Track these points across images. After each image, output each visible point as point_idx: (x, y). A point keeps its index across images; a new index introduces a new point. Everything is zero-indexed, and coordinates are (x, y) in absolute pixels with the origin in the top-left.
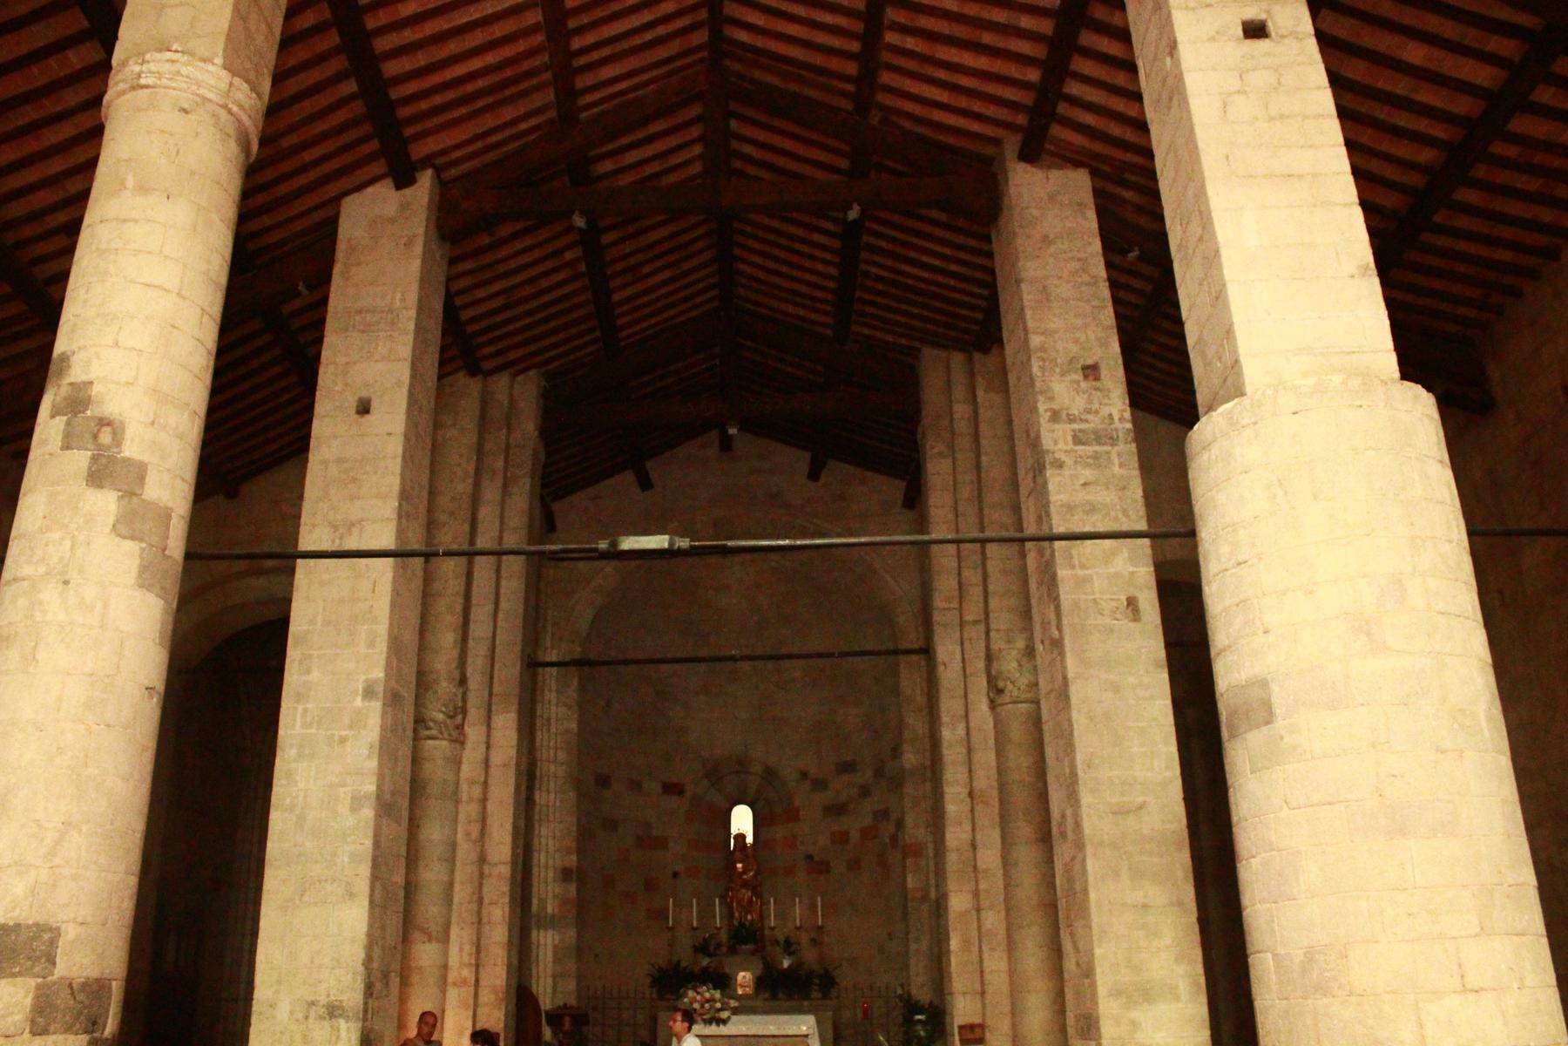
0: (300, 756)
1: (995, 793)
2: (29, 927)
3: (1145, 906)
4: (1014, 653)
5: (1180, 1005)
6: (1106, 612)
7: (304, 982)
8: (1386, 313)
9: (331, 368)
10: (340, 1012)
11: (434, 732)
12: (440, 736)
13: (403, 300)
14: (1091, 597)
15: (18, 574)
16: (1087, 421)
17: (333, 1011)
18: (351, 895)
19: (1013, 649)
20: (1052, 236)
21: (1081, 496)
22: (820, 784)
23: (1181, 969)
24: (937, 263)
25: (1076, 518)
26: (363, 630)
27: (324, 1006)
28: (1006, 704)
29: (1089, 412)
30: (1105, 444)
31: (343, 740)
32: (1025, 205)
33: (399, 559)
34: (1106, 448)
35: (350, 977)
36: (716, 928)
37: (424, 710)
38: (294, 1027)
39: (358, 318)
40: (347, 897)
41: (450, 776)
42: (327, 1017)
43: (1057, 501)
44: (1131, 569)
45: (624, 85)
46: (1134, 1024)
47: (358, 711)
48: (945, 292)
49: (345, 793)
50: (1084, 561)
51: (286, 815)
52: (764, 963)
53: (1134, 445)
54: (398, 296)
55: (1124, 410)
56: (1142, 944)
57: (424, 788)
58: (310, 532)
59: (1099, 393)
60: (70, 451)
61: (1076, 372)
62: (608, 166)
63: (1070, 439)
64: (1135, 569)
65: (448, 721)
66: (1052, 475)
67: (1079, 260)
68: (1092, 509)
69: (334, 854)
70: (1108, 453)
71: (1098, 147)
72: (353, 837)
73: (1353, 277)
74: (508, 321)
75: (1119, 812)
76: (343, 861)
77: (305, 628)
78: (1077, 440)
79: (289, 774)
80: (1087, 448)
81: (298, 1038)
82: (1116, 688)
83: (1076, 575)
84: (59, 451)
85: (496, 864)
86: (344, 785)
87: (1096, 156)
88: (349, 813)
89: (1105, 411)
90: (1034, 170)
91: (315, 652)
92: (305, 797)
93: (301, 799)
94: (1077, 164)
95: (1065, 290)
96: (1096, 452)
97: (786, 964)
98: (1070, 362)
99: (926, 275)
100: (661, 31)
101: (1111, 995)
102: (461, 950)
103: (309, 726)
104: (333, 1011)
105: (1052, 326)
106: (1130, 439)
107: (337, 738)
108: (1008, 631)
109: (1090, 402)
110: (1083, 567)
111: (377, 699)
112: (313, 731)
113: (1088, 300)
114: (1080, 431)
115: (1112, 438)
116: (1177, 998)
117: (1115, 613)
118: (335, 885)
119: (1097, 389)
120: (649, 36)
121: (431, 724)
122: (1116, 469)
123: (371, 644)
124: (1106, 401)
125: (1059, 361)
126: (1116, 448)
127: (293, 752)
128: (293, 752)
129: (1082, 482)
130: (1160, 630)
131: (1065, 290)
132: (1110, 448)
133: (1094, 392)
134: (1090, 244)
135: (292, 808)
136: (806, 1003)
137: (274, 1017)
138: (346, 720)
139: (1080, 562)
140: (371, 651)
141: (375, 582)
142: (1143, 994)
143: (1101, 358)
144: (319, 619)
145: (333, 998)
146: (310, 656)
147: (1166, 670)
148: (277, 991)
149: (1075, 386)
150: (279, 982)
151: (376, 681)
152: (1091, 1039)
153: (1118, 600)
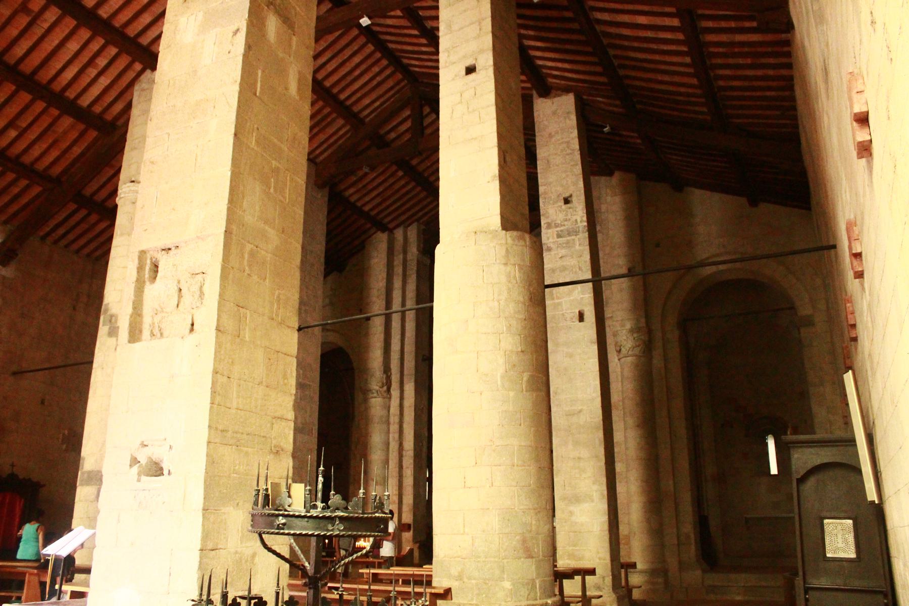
2: (95, 471)
3: (579, 458)
4: (624, 331)
5: (594, 504)
6: (568, 319)
8: (499, 197)
14: (561, 313)
16: (564, 225)
20: (553, 133)
21: (560, 263)
23: (595, 487)
25: (556, 274)
29: (566, 220)
32: (541, 120)
33: (825, 244)
34: (573, 237)
41: (384, 413)
43: (547, 268)
44: (582, 296)
45: (378, 103)
46: (571, 513)
50: (558, 295)
53: (587, 233)
55: (583, 216)
56: (577, 476)
59: (571, 210)
61: (560, 202)
62: (393, 135)
63: (555, 236)
64: (584, 296)
65: (381, 390)
66: (546, 255)
68: (564, 269)
70: (573, 240)
73: (489, 182)
74: (388, 207)
75: (569, 414)
78: (559, 236)
80: (564, 239)
82: (571, 356)
85: (408, 450)
89: (574, 218)
90: (547, 100)
95: (558, 160)
98: (558, 196)
100: (379, 79)
101: (561, 499)
102: (393, 488)
105: (551, 180)
106: (585, 230)
109: (567, 215)
110: (558, 298)
113: (569, 163)
114: (561, 231)
115: (576, 232)
116: (593, 501)
117: (572, 319)
119: (570, 208)
120: (375, 82)
122: (577, 247)
124: (575, 213)
125: (553, 197)
126: (578, 236)
129: (560, 256)
131: (558, 160)
132: (575, 237)
133: (569, 210)
134: (571, 133)
139: (557, 296)
142: (577, 499)
143: (574, 192)
147: (596, 344)
149: (560, 209)
153: (573, 312)
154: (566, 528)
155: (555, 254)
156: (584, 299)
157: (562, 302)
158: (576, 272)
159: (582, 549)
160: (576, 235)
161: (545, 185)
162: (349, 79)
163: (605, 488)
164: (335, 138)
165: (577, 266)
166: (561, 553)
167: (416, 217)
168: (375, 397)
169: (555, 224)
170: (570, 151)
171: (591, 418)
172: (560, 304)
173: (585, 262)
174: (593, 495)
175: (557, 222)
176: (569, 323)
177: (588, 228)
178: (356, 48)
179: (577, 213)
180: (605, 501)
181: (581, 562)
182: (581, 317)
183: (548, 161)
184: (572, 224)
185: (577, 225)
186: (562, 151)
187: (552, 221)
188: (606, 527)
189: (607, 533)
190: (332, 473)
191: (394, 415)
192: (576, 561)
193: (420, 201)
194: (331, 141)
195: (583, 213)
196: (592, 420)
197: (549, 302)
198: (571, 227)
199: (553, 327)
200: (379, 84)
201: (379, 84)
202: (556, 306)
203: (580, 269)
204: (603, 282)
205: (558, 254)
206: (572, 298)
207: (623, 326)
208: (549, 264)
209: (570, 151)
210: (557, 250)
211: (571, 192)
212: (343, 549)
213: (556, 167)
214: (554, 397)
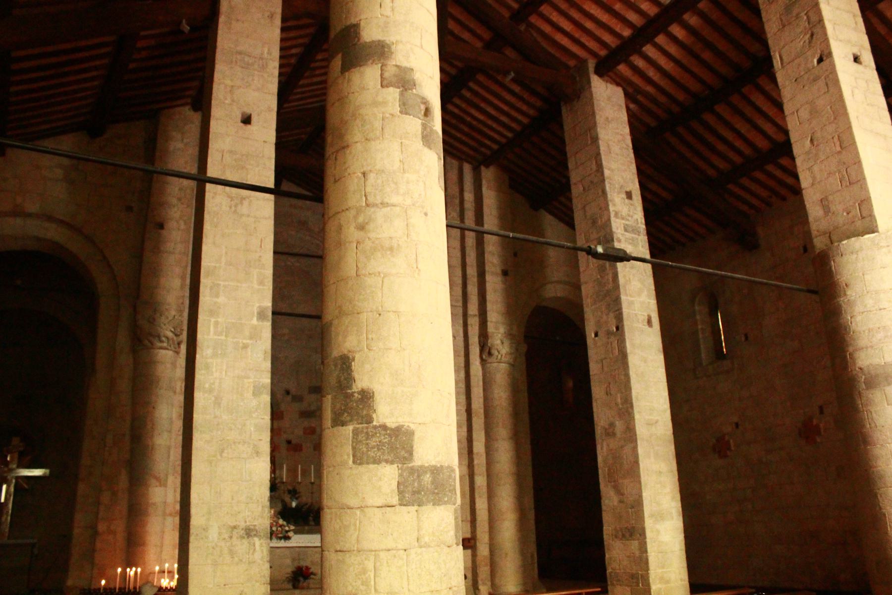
0: (215, 355)
1: (482, 411)
4: (500, 335)
7: (227, 513)
9: (222, 87)
10: (255, 533)
11: (165, 345)
12: (169, 348)
13: (269, 53)
15: (386, 200)
16: (628, 220)
17: (249, 532)
18: (257, 453)
19: (499, 333)
22: (298, 399)
24: (493, 112)
26: (255, 272)
27: (242, 529)
28: (494, 363)
30: (636, 234)
31: (245, 347)
35: (260, 509)
36: (298, 483)
37: (159, 329)
38: (223, 544)
39: (239, 57)
40: (255, 455)
42: (246, 537)
46: (658, 532)
47: (255, 328)
48: (485, 129)
49: (249, 383)
51: (206, 395)
52: (283, 505)
54: (266, 50)
57: (158, 382)
58: (213, 198)
60: (408, 116)
65: (175, 338)
67: (621, 135)
69: (245, 425)
71: (636, 80)
72: (256, 414)
76: (251, 430)
77: (213, 264)
79: (207, 367)
81: (226, 551)
83: (628, 300)
84: (398, 113)
86: (248, 378)
87: (630, 83)
88: (253, 397)
91: (222, 283)
92: (220, 383)
93: (217, 384)
94: (618, 84)
96: (633, 237)
97: (294, 504)
99: (481, 117)
103: (221, 334)
104: (249, 532)
107: (241, 345)
108: (497, 322)
110: (631, 296)
111: (268, 320)
112: (223, 338)
114: (626, 225)
118: (246, 446)
119: (631, 205)
121: (164, 339)
123: (261, 283)
127: (209, 352)
128: (209, 352)
130: (659, 333)
135: (211, 391)
136: (306, 528)
137: (207, 537)
138: (247, 333)
140: (261, 287)
141: (262, 240)
142: (660, 517)
144: (223, 260)
145: (248, 524)
146: (219, 285)
148: (208, 520)
150: (209, 513)
151: (266, 308)
152: (634, 540)
166: (653, 577)
168: (167, 349)
176: (640, 325)
181: (669, 585)
182: (649, 322)
186: (619, 141)
189: (684, 553)
190: (721, 327)
193: (476, 94)
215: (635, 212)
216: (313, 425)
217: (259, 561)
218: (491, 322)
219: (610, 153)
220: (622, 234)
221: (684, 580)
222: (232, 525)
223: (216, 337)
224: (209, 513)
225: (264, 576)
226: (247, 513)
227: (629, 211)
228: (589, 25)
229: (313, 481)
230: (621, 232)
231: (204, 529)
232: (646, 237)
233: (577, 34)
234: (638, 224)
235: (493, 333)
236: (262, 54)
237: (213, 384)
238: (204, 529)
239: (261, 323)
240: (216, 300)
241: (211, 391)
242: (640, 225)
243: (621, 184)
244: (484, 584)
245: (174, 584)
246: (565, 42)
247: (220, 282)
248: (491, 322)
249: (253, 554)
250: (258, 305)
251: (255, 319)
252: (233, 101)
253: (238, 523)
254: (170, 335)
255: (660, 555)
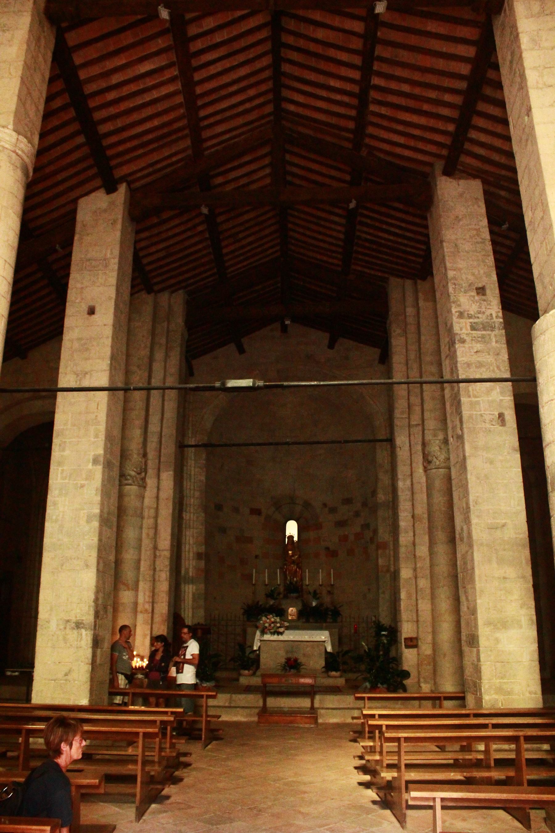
1: (426, 516)
3: (505, 578)
10: (82, 626)
11: (130, 482)
16: (478, 318)
17: (79, 625)
20: (460, 217)
21: (475, 358)
22: (333, 510)
23: (523, 611)
26: (92, 429)
31: (82, 486)
34: (488, 332)
35: (87, 608)
39: (88, 263)
41: (138, 504)
44: (501, 398)
46: (497, 641)
47: (90, 471)
50: (475, 392)
55: (499, 312)
59: (485, 302)
63: (469, 328)
65: (138, 476)
68: (480, 365)
69: (79, 545)
70: (489, 335)
75: (492, 528)
78: (473, 328)
81: (61, 638)
85: (163, 550)
89: (488, 312)
92: (63, 515)
93: (61, 516)
97: (314, 604)
98: (470, 285)
100: (248, 106)
103: (64, 478)
104: (79, 625)
105: (461, 266)
107: (79, 485)
111: (100, 464)
112: (67, 481)
114: (475, 323)
115: (492, 327)
116: (521, 627)
119: (484, 300)
120: (241, 109)
121: (129, 477)
122: (494, 344)
123: (96, 436)
129: (475, 351)
131: (467, 246)
135: (56, 521)
136: (324, 625)
137: (49, 627)
138: (84, 476)
145: (78, 618)
147: (519, 453)
148: (50, 615)
149: (472, 299)
150: (51, 610)
151: (99, 455)
154: (492, 658)
155: (469, 347)
156: (504, 401)
157: (479, 401)
158: (493, 371)
159: (511, 682)
160: (492, 331)
161: (454, 270)
162: (214, 97)
163: (533, 613)
164: (164, 163)
165: (495, 365)
166: (487, 687)
167: (183, 284)
168: (131, 485)
169: (468, 314)
170: (480, 240)
171: (516, 533)
172: (478, 403)
173: (503, 361)
174: (521, 621)
175: (469, 313)
176: (488, 426)
177: (504, 325)
178: (251, 56)
179: (491, 307)
180: (535, 627)
183: (456, 245)
184: (487, 318)
185: (492, 320)
186: (471, 237)
187: (465, 311)
188: (536, 656)
191: (149, 508)
192: (504, 696)
194: (159, 166)
195: (499, 308)
196: (518, 536)
197: (465, 399)
198: (485, 321)
199: (469, 428)
200: (247, 111)
201: (247, 111)
202: (473, 405)
203: (498, 367)
204: (59, 394)
205: (472, 348)
206: (490, 398)
207: (435, 436)
208: (463, 357)
209: (480, 240)
210: (472, 343)
211: (484, 284)
212: (122, 674)
213: (465, 254)
214: (474, 506)
215: (488, 307)
216: (346, 533)
217: (85, 647)
218: (429, 430)
219: (459, 252)
220: (467, 334)
221: (535, 693)
222: (66, 619)
223: (62, 481)
224: (51, 610)
225: (87, 658)
226: (78, 611)
227: (480, 307)
228: (417, 132)
229: (267, 583)
230: (466, 332)
231: (47, 622)
232: (503, 331)
233: (412, 143)
234: (492, 318)
235: (430, 441)
236: (105, 255)
237: (59, 516)
238: (47, 622)
239: (94, 467)
240: (62, 453)
241: (56, 521)
242: (495, 319)
243: (470, 282)
244: (426, 682)
245: (145, 663)
246: (407, 153)
247: (66, 440)
248: (429, 430)
249: (80, 641)
250: (93, 453)
251: (91, 464)
252: (82, 299)
253: (71, 618)
254: (133, 473)
255: (498, 665)
